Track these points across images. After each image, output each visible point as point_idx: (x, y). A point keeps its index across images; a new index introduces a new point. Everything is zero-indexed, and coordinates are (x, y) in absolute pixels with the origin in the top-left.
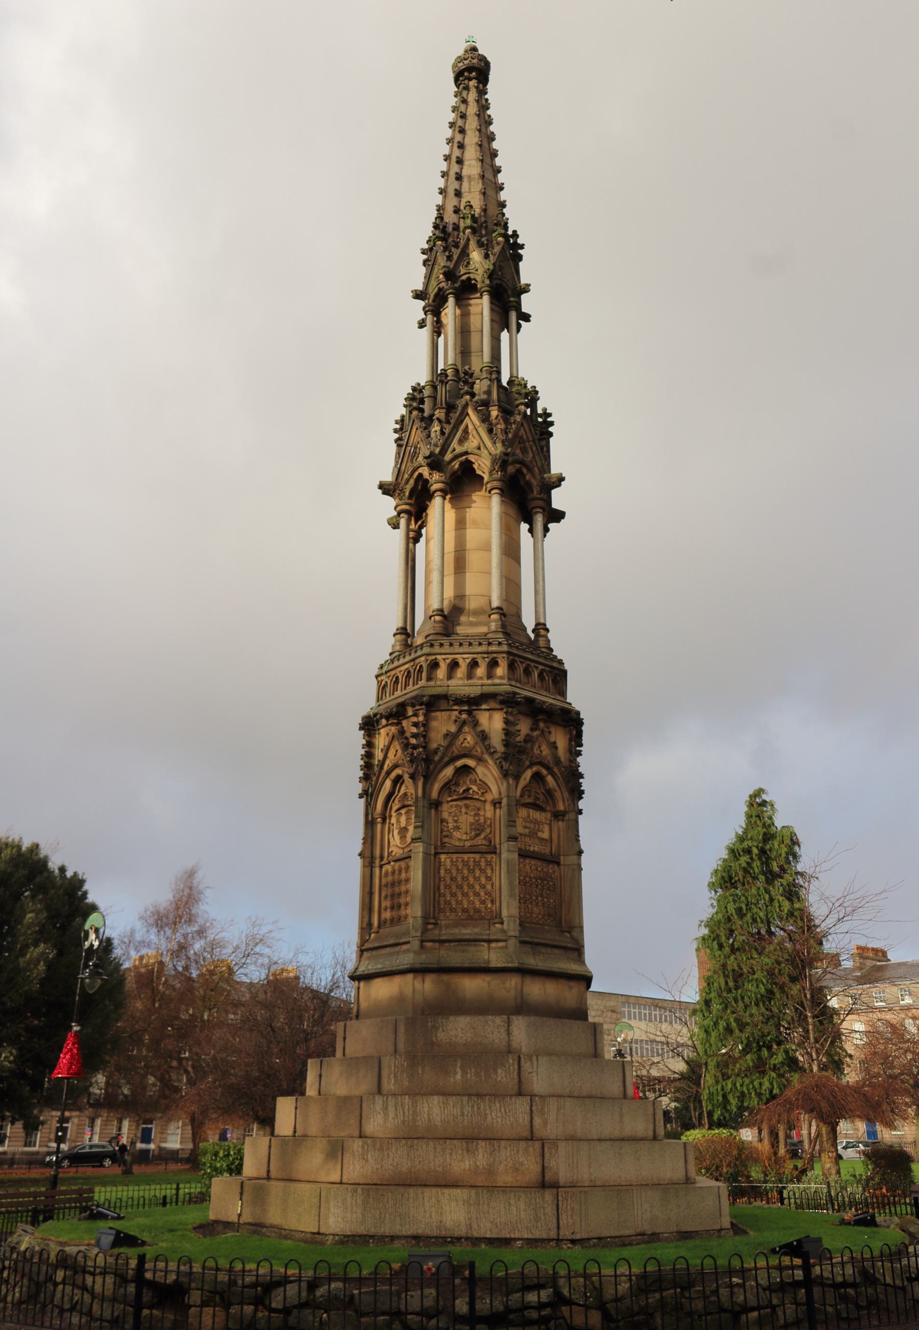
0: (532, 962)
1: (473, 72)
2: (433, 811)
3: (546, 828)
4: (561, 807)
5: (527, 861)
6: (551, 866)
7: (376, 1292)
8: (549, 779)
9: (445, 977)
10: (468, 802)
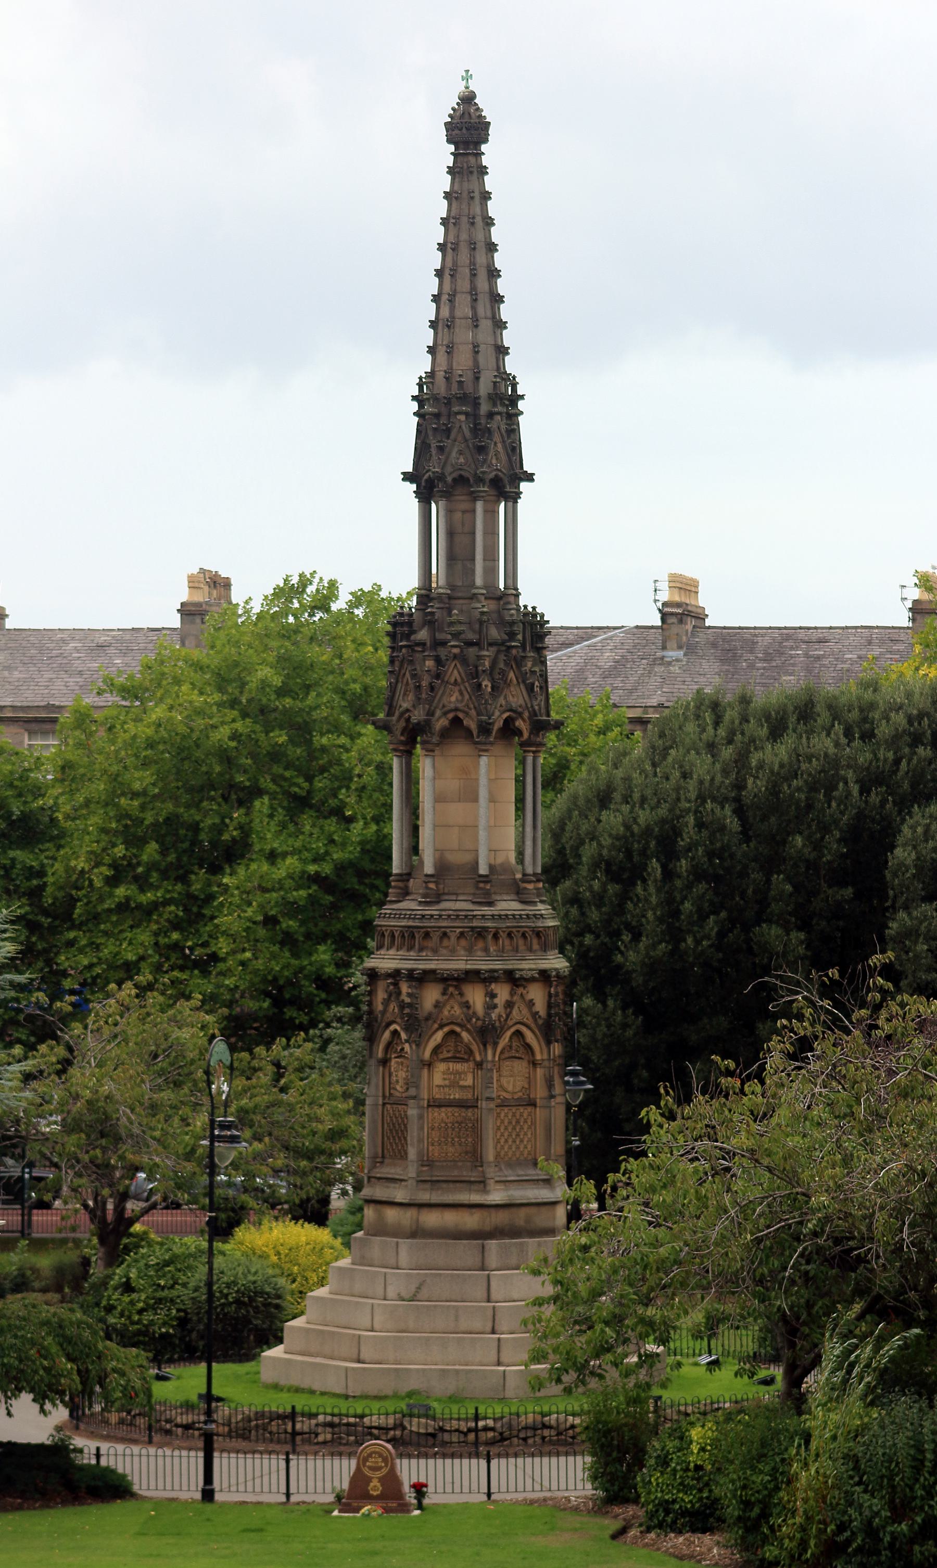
1: (467, 130)
2: (381, 1068)
4: (478, 1058)
5: (443, 1109)
8: (465, 1035)
9: (379, 1207)
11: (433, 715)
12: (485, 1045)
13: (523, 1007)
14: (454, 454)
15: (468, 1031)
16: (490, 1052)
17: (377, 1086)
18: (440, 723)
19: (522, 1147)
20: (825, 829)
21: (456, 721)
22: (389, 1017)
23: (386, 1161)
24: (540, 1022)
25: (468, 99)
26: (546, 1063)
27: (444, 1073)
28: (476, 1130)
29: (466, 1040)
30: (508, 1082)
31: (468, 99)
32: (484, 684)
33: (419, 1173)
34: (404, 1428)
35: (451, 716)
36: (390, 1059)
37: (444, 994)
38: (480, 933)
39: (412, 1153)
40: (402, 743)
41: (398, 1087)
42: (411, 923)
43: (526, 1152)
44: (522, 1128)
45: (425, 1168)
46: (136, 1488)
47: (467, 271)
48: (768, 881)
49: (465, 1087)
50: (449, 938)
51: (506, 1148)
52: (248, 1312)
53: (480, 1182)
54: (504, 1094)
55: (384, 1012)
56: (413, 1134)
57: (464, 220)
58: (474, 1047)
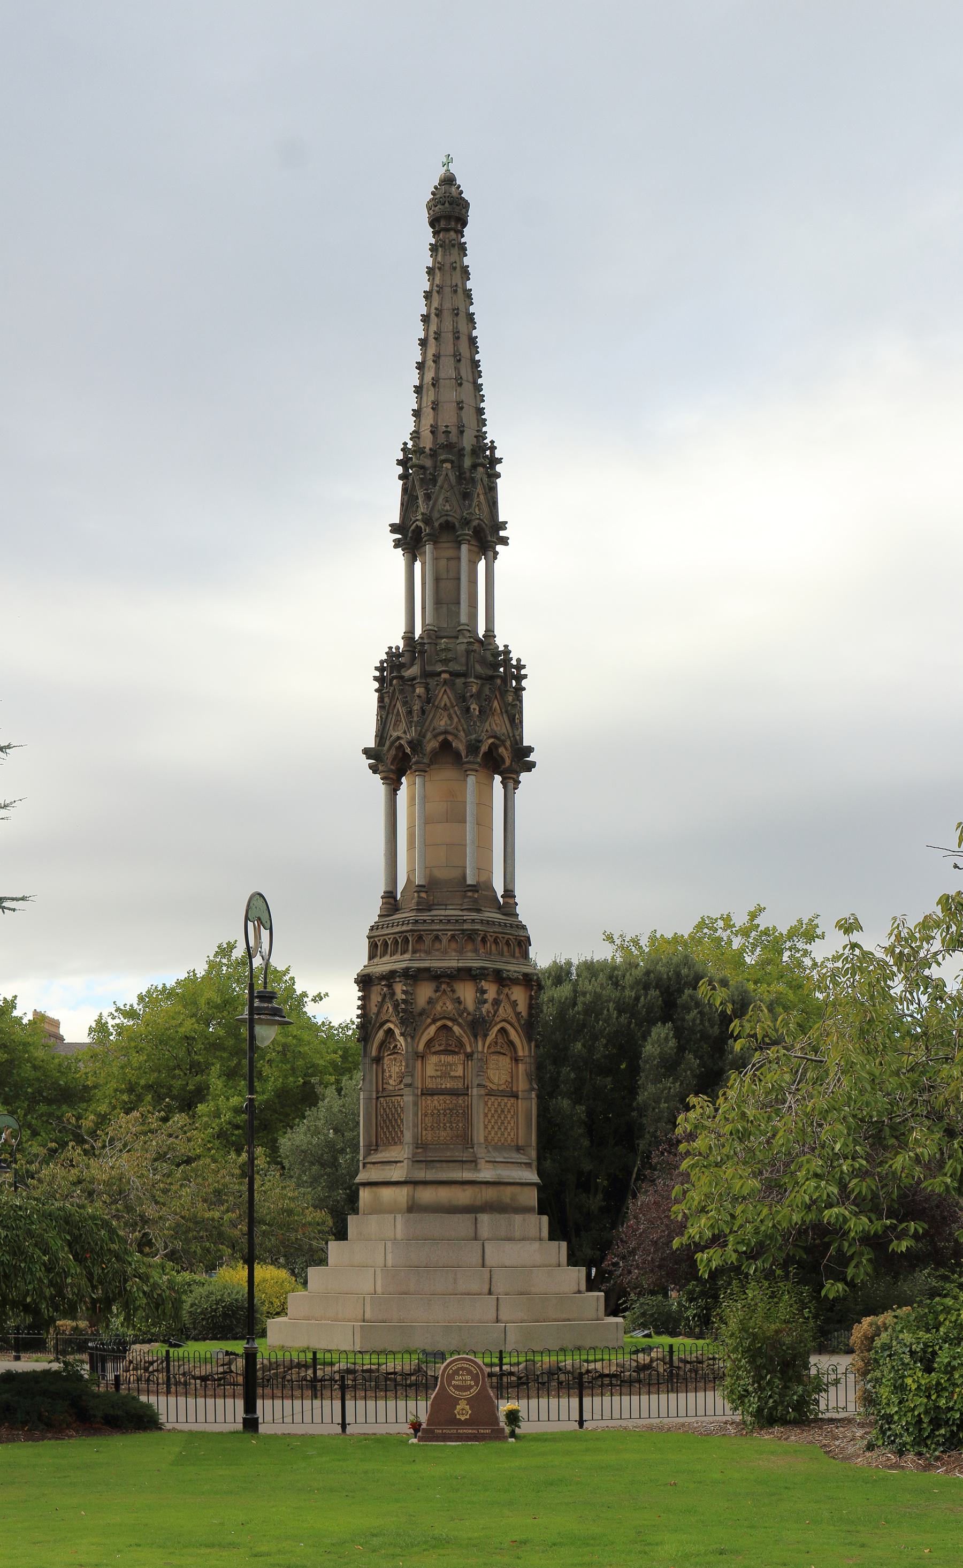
0: (421, 1175)
1: (449, 213)
3: (460, 1068)
4: (469, 1050)
5: (436, 1097)
6: (461, 1098)
8: (456, 1029)
9: (375, 1189)
10: (395, 1056)
11: (424, 737)
12: (475, 1037)
14: (440, 501)
15: (459, 1025)
16: (480, 1043)
17: (371, 1081)
18: (431, 745)
19: (506, 1134)
20: (595, 1038)
21: (446, 746)
22: (384, 1017)
23: (380, 1148)
24: (523, 1022)
25: (448, 180)
26: (528, 1060)
27: (436, 1065)
28: (467, 1115)
29: (457, 1034)
31: (448, 180)
32: (472, 707)
33: (414, 1155)
35: (441, 738)
36: (383, 1057)
37: (436, 991)
38: (470, 936)
39: (408, 1136)
40: (392, 771)
41: (391, 1082)
42: (405, 928)
43: (509, 1139)
44: (506, 1117)
45: (420, 1150)
46: (162, 1419)
47: (450, 336)
48: (559, 1073)
49: (456, 1077)
50: (440, 941)
51: (493, 1133)
52: (231, 1322)
53: (472, 1161)
54: (491, 1085)
56: (408, 1118)
57: (447, 290)
58: (465, 1040)
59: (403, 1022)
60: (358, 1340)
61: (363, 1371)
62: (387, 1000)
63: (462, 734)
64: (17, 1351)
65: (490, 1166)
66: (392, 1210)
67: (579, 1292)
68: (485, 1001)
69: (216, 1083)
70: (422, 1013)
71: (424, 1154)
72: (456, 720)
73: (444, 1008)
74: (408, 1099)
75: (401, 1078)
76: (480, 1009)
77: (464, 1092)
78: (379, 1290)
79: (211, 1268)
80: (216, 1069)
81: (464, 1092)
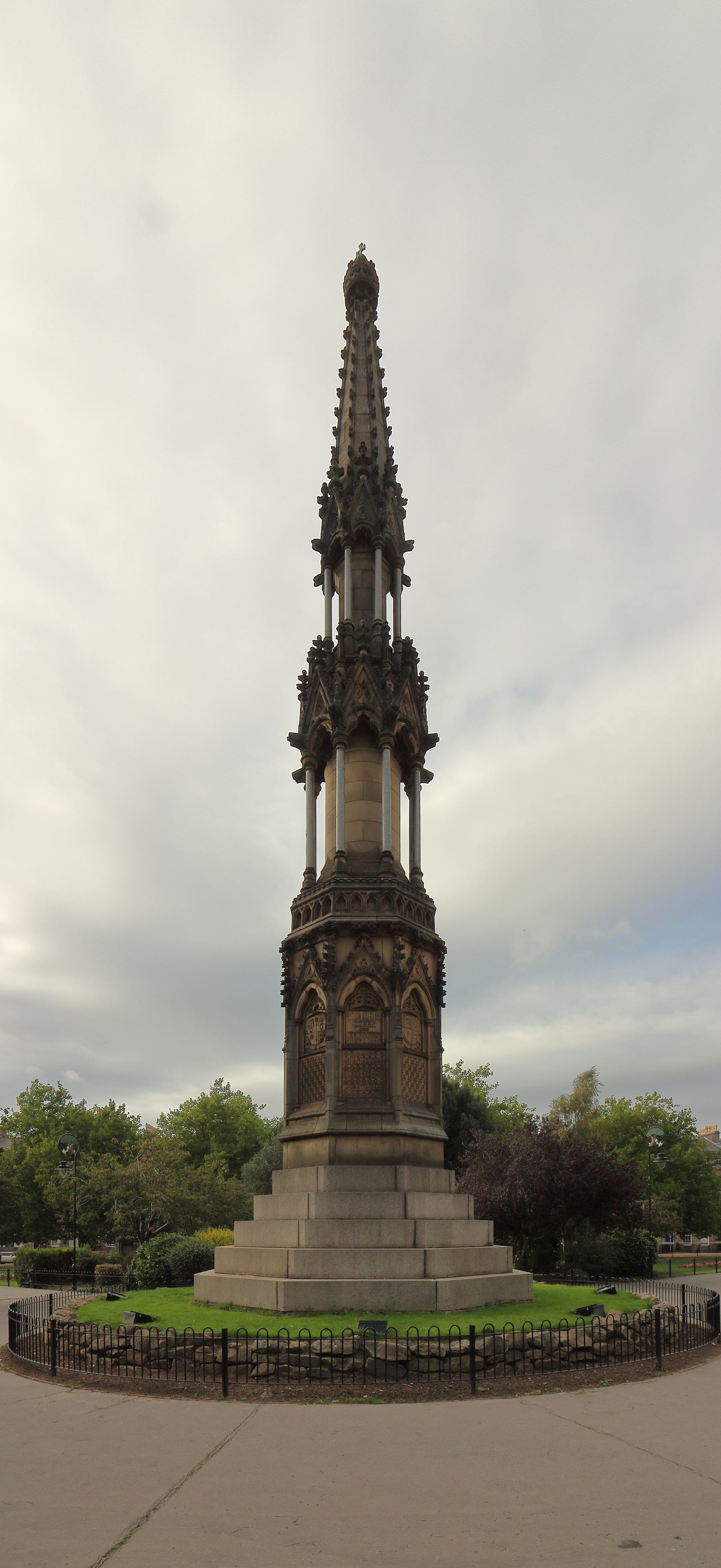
0: (342, 1127)
1: (362, 286)
2: (297, 1028)
5: (355, 1052)
6: (379, 1053)
7: (185, 1346)
9: (297, 1144)
12: (393, 990)
13: (420, 969)
15: (378, 980)
16: (397, 998)
28: (385, 1071)
29: (376, 989)
30: (408, 1033)
32: (388, 682)
34: (366, 1354)
35: (359, 714)
36: (305, 1020)
37: (356, 947)
39: (330, 1088)
45: (341, 1103)
47: (364, 380)
49: (374, 1033)
55: (302, 975)
58: (383, 996)
59: (326, 976)
60: (281, 1299)
61: (289, 1351)
62: (310, 960)
63: (379, 708)
64: (75, 1284)
65: (406, 1118)
66: (314, 1162)
67: (489, 1244)
68: (403, 957)
69: (214, 1145)
70: (344, 968)
71: (345, 1108)
72: (373, 695)
73: (364, 964)
74: (330, 1052)
75: (323, 1036)
76: (397, 964)
77: (382, 1047)
78: (303, 1243)
79: (191, 1233)
80: (213, 1138)
81: (382, 1047)
